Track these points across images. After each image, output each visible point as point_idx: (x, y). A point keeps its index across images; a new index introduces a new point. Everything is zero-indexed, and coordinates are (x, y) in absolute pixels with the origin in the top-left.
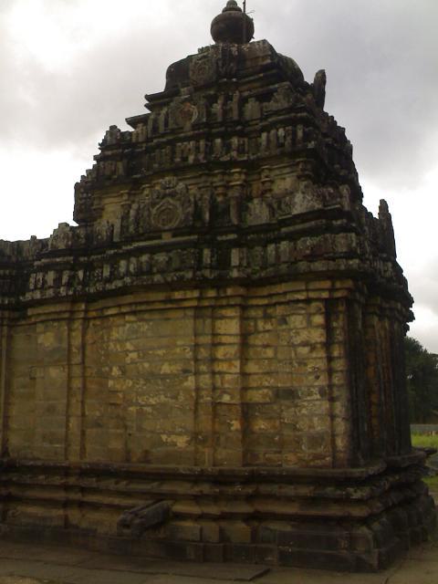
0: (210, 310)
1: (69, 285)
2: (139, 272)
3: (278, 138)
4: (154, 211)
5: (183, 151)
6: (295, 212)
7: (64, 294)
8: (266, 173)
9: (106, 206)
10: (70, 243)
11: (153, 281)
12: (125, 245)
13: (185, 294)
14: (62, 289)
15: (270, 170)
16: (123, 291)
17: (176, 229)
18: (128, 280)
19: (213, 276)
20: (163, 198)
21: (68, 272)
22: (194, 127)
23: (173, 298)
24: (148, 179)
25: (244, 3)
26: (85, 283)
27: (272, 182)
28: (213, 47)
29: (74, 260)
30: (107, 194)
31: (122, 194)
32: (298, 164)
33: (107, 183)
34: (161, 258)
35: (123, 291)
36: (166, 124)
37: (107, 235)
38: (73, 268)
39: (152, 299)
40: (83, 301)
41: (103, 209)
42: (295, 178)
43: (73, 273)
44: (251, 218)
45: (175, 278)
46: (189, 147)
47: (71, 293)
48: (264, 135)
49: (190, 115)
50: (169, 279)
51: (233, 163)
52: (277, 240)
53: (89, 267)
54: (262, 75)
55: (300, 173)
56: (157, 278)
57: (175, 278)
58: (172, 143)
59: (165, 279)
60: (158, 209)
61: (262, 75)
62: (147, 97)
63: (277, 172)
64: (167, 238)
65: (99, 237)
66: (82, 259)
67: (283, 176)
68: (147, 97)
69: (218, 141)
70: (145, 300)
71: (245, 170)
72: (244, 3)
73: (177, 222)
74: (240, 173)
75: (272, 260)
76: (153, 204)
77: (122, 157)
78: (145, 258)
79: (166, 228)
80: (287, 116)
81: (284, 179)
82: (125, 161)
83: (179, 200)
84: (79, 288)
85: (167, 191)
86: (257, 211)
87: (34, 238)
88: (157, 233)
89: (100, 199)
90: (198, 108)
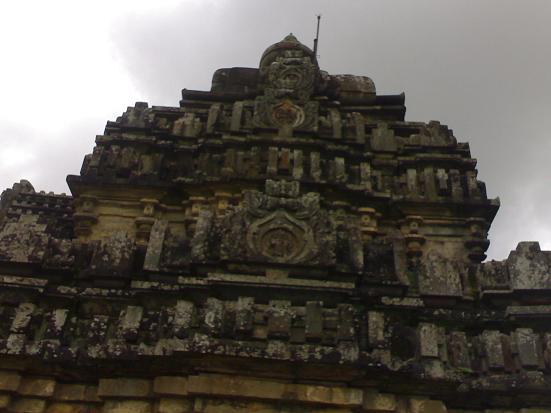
0: (42, 404)
1: (28, 333)
2: (227, 331)
3: (437, 181)
4: (254, 226)
5: (279, 160)
6: (520, 286)
7: (15, 350)
8: (414, 226)
9: (100, 218)
10: (41, 253)
11: (264, 353)
12: (185, 275)
13: (331, 394)
14: (12, 338)
15: (421, 224)
16: (177, 365)
17: (299, 266)
18: (203, 341)
19: (398, 366)
20: (272, 209)
21: (32, 307)
22: (296, 133)
23: (301, 398)
24: (207, 189)
25: (316, 41)
26: (65, 336)
27: (422, 241)
28: (63, 197)
29: (46, 288)
30: (109, 198)
31: (145, 204)
32: (468, 225)
33: (120, 181)
34: (281, 310)
35: (177, 365)
36: (243, 122)
37: (123, 259)
38: (48, 300)
39: (251, 394)
40: (47, 376)
41: (95, 221)
42: (461, 245)
43: (40, 311)
44: (428, 282)
45: (318, 356)
46: (290, 156)
47: (34, 350)
48: (412, 173)
49: (291, 117)
50: (304, 356)
51: (362, 198)
52: (508, 326)
53: (74, 306)
54: (378, 107)
55: (470, 239)
56: (274, 348)
57: (318, 356)
58: (264, 145)
59: (293, 353)
60: (260, 226)
61: (378, 107)
62: (185, 92)
63: (430, 231)
64: (275, 278)
65: (106, 258)
66: (63, 289)
67: (440, 239)
68: (185, 92)
69: (340, 161)
70: (233, 392)
71: (379, 214)
72: (316, 41)
73: (303, 255)
74: (371, 215)
75: (497, 358)
76: (254, 217)
77: (151, 149)
78: (243, 304)
79: (281, 260)
80: (449, 156)
81: (442, 243)
82: (160, 156)
83: (307, 219)
84: (54, 344)
85: (283, 201)
86: (438, 273)
87: (109, 124)
88: (260, 265)
89: (96, 203)
90: (306, 110)
